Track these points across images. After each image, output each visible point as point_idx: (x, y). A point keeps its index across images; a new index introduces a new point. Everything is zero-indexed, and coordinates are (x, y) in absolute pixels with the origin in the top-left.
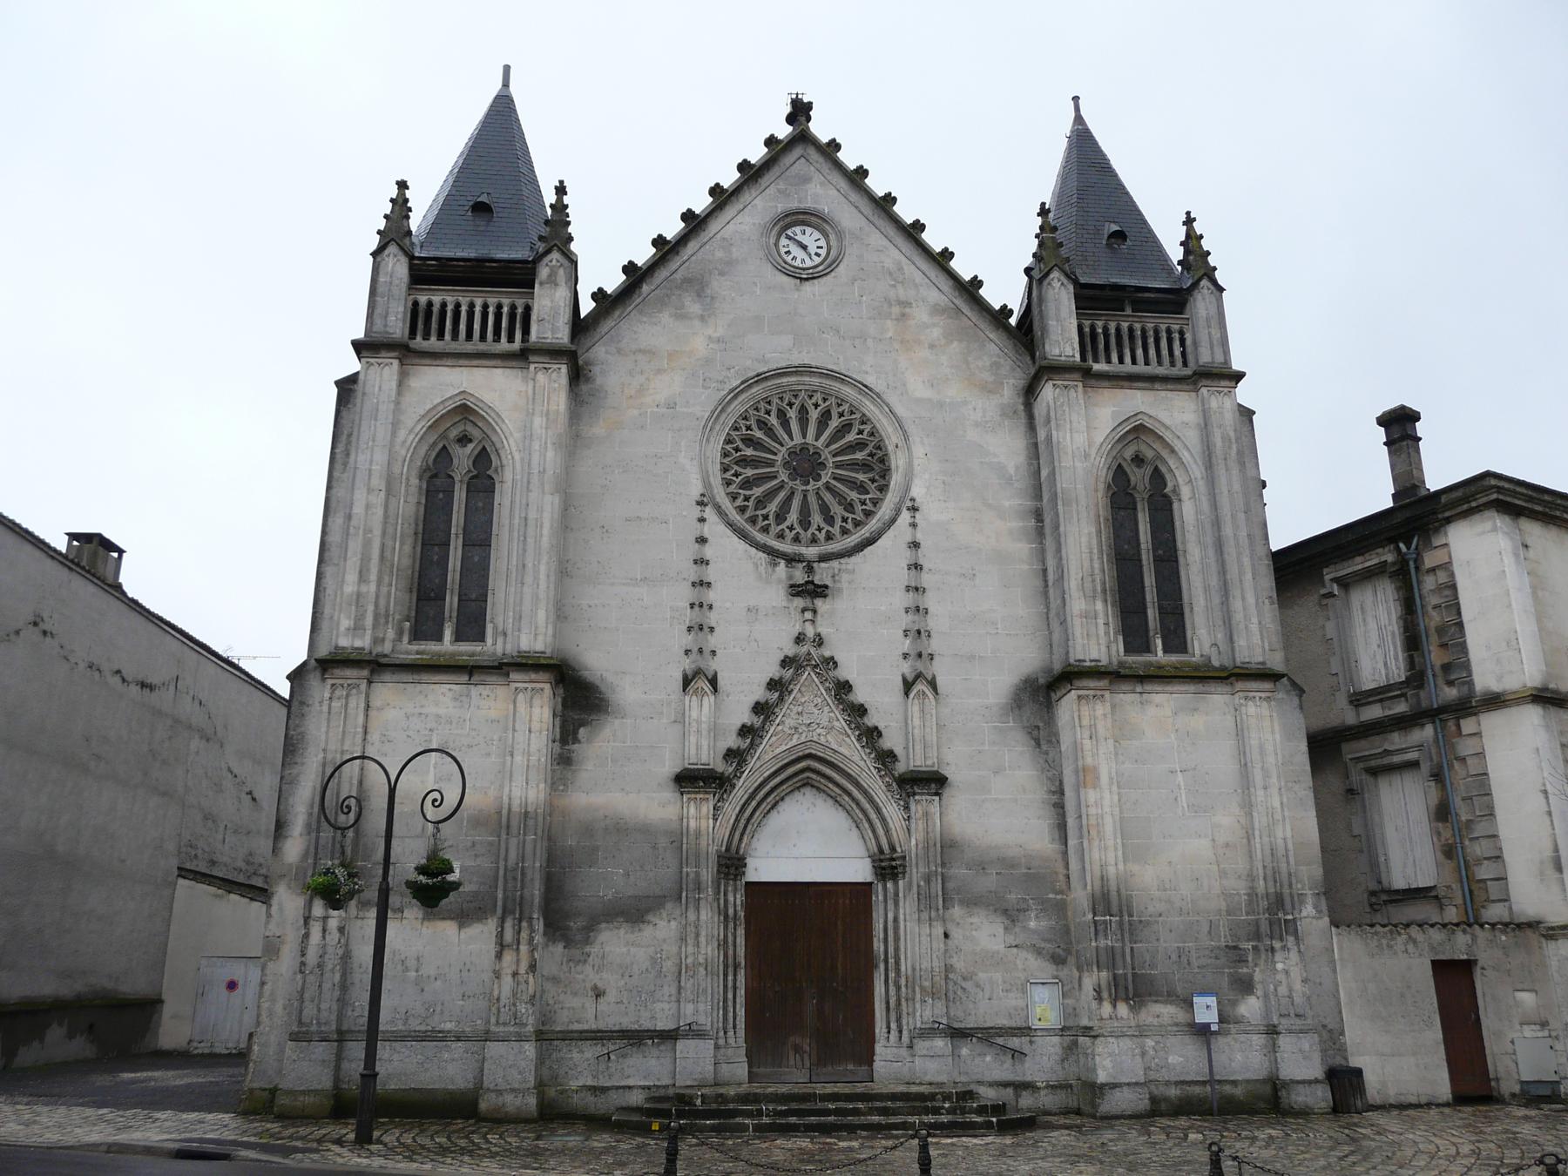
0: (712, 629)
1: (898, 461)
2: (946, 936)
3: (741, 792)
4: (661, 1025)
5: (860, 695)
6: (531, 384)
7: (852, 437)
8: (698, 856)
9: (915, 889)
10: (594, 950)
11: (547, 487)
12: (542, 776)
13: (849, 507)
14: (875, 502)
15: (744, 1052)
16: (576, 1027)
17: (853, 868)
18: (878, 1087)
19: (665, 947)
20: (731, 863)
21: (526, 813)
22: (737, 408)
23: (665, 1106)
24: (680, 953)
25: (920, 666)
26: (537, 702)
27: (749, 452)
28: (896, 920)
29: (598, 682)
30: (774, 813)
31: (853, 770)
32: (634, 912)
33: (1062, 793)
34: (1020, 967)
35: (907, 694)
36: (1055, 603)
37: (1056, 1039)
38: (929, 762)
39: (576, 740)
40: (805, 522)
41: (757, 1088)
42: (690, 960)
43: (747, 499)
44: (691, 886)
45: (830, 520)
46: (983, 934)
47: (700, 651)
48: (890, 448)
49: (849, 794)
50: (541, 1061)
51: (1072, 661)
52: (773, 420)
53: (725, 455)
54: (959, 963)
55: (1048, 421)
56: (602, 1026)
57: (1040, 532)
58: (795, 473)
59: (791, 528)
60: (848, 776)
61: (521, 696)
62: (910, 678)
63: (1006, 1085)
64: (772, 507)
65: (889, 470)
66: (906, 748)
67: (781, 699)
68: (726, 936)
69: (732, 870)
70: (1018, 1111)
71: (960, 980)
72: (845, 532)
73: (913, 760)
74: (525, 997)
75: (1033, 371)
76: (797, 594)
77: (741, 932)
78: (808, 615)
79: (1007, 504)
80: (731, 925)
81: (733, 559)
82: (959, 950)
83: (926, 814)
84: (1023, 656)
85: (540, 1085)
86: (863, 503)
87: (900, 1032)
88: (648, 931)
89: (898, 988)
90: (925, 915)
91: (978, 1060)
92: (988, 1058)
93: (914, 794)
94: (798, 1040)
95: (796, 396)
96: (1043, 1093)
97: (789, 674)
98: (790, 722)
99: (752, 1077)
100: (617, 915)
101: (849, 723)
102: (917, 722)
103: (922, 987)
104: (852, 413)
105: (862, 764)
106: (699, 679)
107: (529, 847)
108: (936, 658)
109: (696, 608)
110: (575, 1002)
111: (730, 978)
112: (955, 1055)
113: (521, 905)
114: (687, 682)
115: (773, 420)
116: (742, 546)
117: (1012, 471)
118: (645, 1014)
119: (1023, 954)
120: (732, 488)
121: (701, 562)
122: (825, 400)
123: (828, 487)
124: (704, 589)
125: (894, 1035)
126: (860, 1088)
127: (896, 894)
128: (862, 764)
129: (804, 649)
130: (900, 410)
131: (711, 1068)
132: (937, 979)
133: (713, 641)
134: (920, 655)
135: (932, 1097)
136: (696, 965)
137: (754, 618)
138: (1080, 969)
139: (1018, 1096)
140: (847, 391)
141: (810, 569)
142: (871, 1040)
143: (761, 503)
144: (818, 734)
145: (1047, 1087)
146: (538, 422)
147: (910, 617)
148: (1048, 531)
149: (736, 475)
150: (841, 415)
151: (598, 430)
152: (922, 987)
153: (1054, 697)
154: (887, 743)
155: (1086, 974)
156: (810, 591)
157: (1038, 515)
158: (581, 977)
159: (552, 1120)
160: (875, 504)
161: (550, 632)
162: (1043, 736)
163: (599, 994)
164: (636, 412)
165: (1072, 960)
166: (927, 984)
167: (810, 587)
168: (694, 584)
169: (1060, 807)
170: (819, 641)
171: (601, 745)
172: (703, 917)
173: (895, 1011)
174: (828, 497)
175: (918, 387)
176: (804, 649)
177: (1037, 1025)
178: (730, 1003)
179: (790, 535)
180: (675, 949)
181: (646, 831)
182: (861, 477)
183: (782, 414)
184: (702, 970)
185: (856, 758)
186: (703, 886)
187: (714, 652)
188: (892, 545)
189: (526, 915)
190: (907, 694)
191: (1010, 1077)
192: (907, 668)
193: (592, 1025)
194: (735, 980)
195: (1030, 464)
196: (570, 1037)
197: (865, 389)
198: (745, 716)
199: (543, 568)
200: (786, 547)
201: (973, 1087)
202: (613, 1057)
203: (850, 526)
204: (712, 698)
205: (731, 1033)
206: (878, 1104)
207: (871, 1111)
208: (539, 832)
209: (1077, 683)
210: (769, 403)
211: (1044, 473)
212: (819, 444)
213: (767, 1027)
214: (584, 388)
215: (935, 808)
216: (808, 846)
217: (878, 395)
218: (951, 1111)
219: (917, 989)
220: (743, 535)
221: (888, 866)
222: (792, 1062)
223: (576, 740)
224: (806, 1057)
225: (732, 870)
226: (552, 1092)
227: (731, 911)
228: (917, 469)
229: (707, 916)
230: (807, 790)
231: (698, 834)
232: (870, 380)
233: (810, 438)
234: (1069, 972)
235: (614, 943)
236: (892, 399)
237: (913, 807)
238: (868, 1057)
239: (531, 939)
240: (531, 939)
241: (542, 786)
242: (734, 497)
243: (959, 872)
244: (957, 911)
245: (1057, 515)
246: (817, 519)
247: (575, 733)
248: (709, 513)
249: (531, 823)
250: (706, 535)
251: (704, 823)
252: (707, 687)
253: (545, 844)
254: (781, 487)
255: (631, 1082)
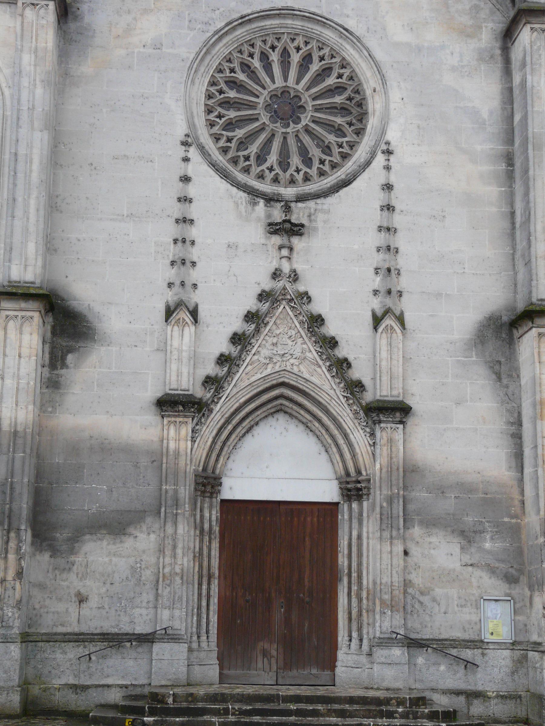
0: (194, 264)
1: (375, 105)
2: (406, 553)
3: (218, 416)
4: (139, 629)
5: (331, 329)
6: (19, 19)
7: (331, 81)
8: (176, 474)
9: (378, 509)
10: (79, 559)
11: (36, 124)
12: (31, 398)
13: (327, 149)
14: (352, 146)
15: (215, 655)
16: (61, 629)
17: (322, 489)
18: (339, 691)
19: (144, 557)
20: (208, 482)
21: (15, 433)
22: (222, 50)
23: (139, 704)
24: (158, 563)
25: (389, 302)
26: (27, 329)
27: (232, 94)
28: (359, 537)
29: (85, 312)
30: (249, 437)
31: (323, 398)
32: (116, 525)
33: (520, 424)
34: (475, 584)
35: (376, 328)
36: (521, 245)
37: (507, 653)
38: (395, 393)
39: (64, 365)
40: (284, 164)
41: (226, 689)
42: (167, 570)
43: (229, 140)
44: (169, 502)
45: (308, 161)
46: (440, 553)
47: (183, 284)
48: (368, 92)
49: (319, 421)
50: (25, 661)
51: (534, 300)
52: (256, 63)
53: (210, 97)
54: (417, 579)
55: (524, 65)
56: (84, 629)
57: (510, 176)
58: (276, 116)
59: (271, 169)
60: (319, 404)
61: (11, 324)
62: (379, 313)
63: (458, 693)
64: (254, 149)
65: (366, 113)
66: (374, 379)
67: (258, 330)
68: (201, 549)
69: (209, 488)
70: (469, 718)
71: (417, 595)
72: (322, 174)
73: (379, 390)
74: (12, 602)
75: (512, 13)
76: (275, 232)
77: (215, 545)
78: (285, 252)
79: (479, 148)
80: (206, 538)
81: (214, 195)
82: (417, 567)
83: (391, 441)
84: (490, 295)
85: (25, 685)
86: (340, 146)
87: (361, 640)
88: (129, 542)
89: (360, 600)
90: (386, 534)
91: (432, 669)
92: (442, 668)
93: (380, 422)
94: (266, 646)
95: (278, 39)
96: (493, 702)
97: (265, 307)
98: (265, 352)
99: (222, 678)
100: (100, 527)
101: (321, 354)
102: (384, 354)
103: (382, 602)
104: (333, 57)
105: (331, 392)
106: (181, 310)
107: (18, 464)
108: (405, 295)
109: (180, 244)
110: (60, 607)
111: (204, 587)
112: (411, 663)
113: (9, 517)
114: (169, 313)
115: (256, 63)
116: (223, 185)
117: (485, 114)
118: (125, 619)
119: (478, 573)
120: (216, 129)
121: (185, 200)
122: (306, 43)
123: (307, 130)
124: (187, 226)
125: (355, 643)
126: (321, 691)
127: (361, 514)
128: (331, 392)
129: (280, 284)
130: (379, 55)
131: (185, 669)
132: (396, 592)
133: (194, 275)
134: (389, 292)
135: (387, 702)
136: (173, 574)
137: (234, 252)
138: (531, 588)
139: (469, 704)
140: (329, 35)
141: (287, 209)
142: (334, 647)
143: (243, 144)
144: (291, 364)
145: (497, 696)
146: (27, 59)
147: (381, 256)
148: (518, 174)
149: (220, 116)
150: (322, 59)
151: (85, 68)
152: (382, 602)
153: (516, 334)
154: (355, 374)
155: (537, 593)
156: (288, 230)
157: (509, 159)
158: (65, 584)
159: (35, 716)
160: (351, 147)
161: (40, 263)
162: (503, 371)
163: (82, 600)
164: (123, 52)
165: (524, 579)
166: (386, 597)
167: (287, 226)
168: (177, 221)
169: (517, 438)
170: (294, 277)
171: (88, 370)
172: (180, 531)
173: (356, 621)
174: (307, 140)
175: (398, 33)
176: (280, 284)
177: (489, 638)
178: (204, 610)
179: (269, 176)
180: (153, 560)
181: (128, 450)
182: (339, 120)
183: (264, 57)
184: (178, 580)
185: (326, 387)
186: (181, 502)
187: (195, 286)
188: (366, 186)
189: (15, 525)
190: (376, 328)
191: (462, 686)
192: (377, 304)
193: (74, 628)
194: (209, 589)
195: (503, 109)
196: (52, 638)
197: (346, 32)
198: (223, 346)
199: (33, 202)
200: (266, 187)
201: (427, 694)
202: (93, 658)
203: (327, 168)
204: (193, 328)
205: (204, 638)
206: (336, 707)
207: (330, 713)
208: (28, 451)
209: (539, 321)
210: (252, 46)
211: (517, 118)
212: (300, 87)
213: (238, 631)
214: (72, 26)
215: (399, 436)
216: (280, 468)
217: (358, 39)
218: (405, 716)
219: (378, 602)
220: (225, 175)
221: (354, 488)
222: (260, 665)
223: (64, 365)
224: (273, 661)
225: (209, 488)
226: (35, 690)
227: (206, 526)
228: (393, 113)
229: (184, 530)
230: (281, 417)
231: (177, 454)
232: (351, 24)
233: (291, 82)
234: (521, 590)
235: (98, 553)
236: (372, 43)
237: (378, 434)
238: (330, 663)
239: (19, 549)
240: (19, 549)
241: (31, 407)
242: (217, 138)
243: (420, 495)
244: (417, 531)
245: (527, 159)
246: (295, 160)
247: (63, 359)
248: (193, 153)
249: (20, 441)
250: (190, 174)
251: (182, 445)
252: (188, 318)
253: (34, 460)
254: (262, 129)
255: (110, 681)
